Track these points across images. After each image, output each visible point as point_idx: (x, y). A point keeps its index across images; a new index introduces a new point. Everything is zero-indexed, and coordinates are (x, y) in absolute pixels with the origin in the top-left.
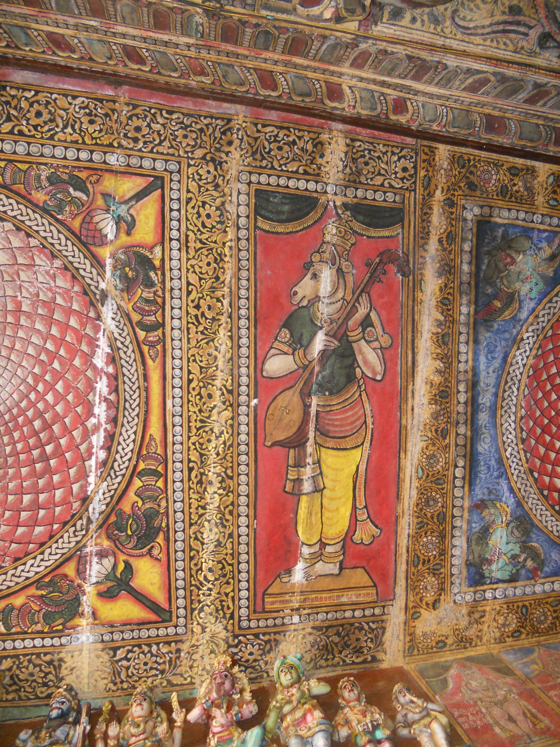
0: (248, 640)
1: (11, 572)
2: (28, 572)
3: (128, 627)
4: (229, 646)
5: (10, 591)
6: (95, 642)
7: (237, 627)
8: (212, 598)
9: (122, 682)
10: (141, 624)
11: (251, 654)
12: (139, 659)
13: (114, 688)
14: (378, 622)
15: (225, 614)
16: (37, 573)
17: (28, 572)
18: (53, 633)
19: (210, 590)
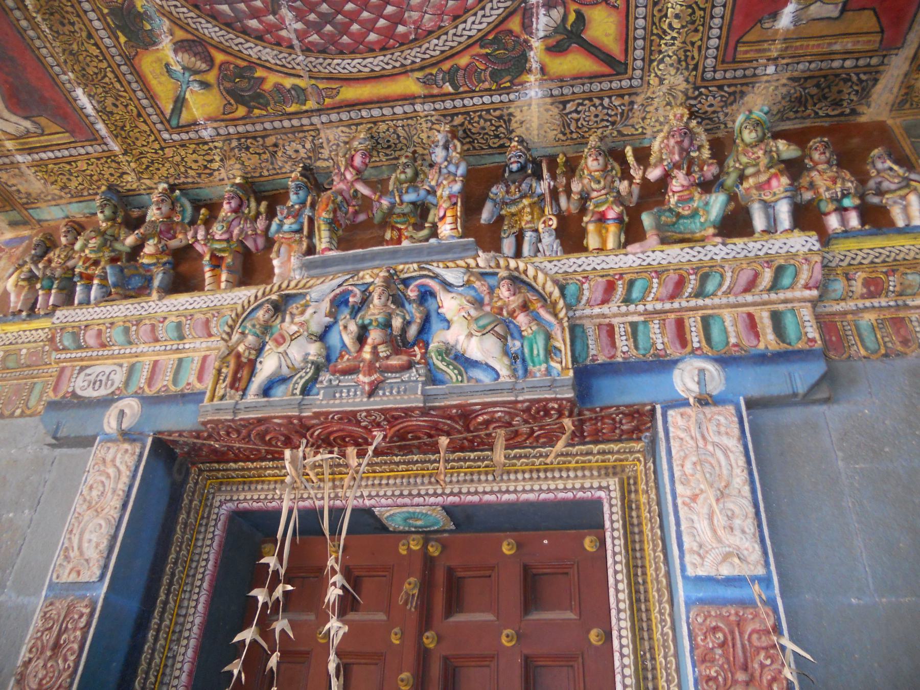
0: (710, 91)
1: (451, 32)
2: (470, 30)
3: (579, 81)
4: (688, 98)
5: (454, 51)
6: (545, 97)
7: (699, 79)
8: (675, 48)
9: (572, 132)
10: (593, 77)
11: (711, 105)
12: (589, 112)
13: (564, 138)
14: (871, 73)
15: (687, 64)
16: (479, 30)
17: (470, 30)
18: (500, 90)
19: (674, 38)
